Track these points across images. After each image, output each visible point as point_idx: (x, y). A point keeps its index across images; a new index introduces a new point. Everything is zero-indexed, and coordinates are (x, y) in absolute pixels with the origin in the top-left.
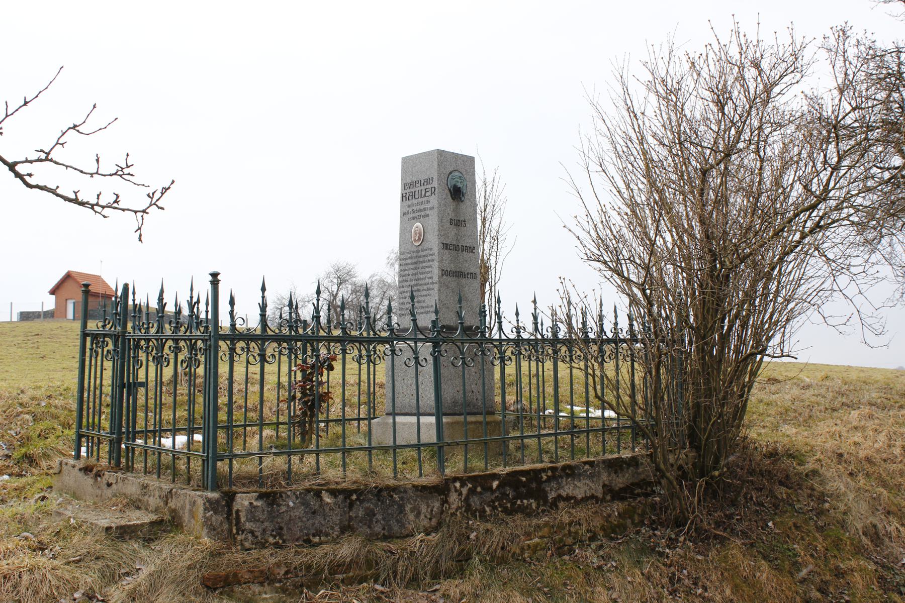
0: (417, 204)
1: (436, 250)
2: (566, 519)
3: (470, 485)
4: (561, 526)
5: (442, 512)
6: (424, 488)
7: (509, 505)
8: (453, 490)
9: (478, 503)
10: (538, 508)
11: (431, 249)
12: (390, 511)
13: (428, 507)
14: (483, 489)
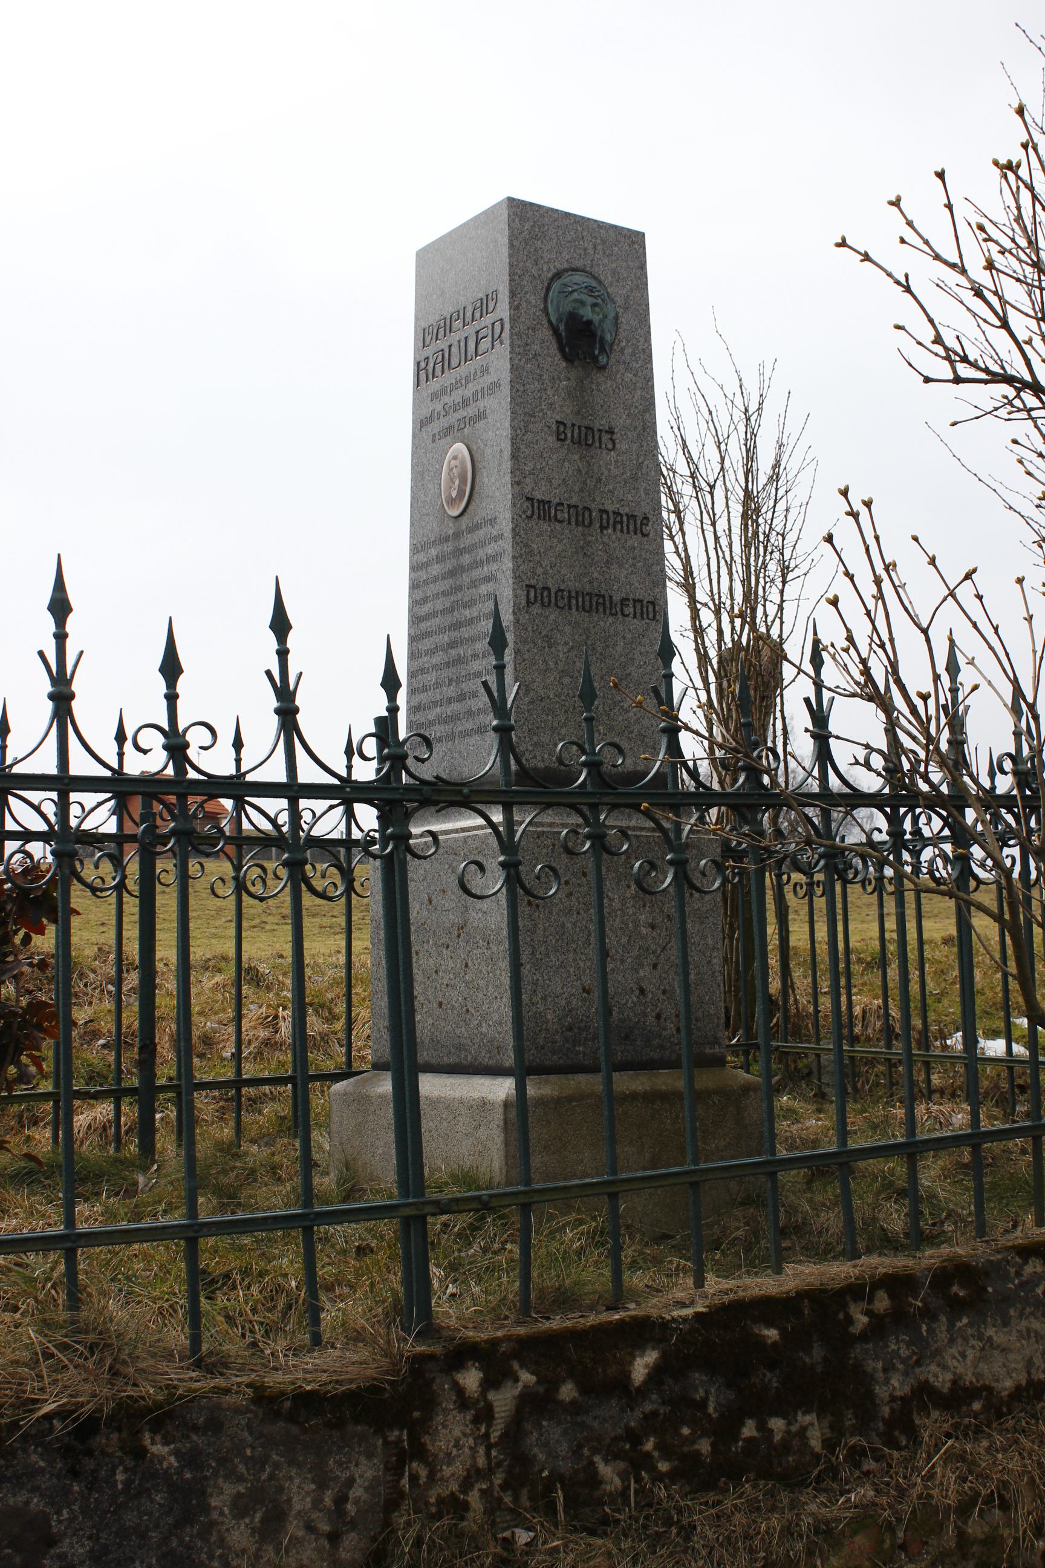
0: (455, 386)
1: (505, 524)
2: (948, 1487)
3: (526, 1377)
4: (927, 1519)
5: (393, 1502)
6: (308, 1402)
7: (704, 1446)
8: (448, 1402)
9: (563, 1449)
10: (830, 1445)
11: (492, 521)
12: (130, 1518)
13: (322, 1486)
14: (585, 1389)
